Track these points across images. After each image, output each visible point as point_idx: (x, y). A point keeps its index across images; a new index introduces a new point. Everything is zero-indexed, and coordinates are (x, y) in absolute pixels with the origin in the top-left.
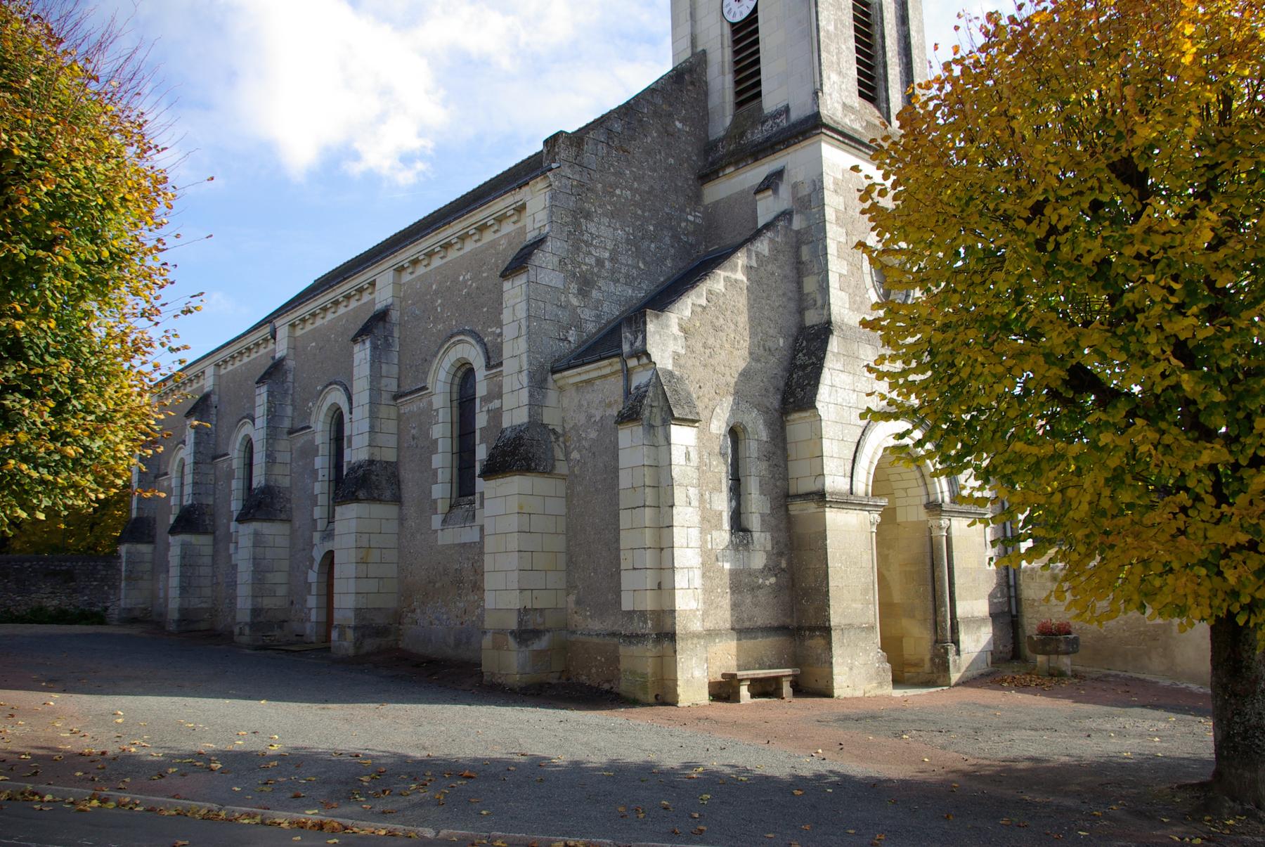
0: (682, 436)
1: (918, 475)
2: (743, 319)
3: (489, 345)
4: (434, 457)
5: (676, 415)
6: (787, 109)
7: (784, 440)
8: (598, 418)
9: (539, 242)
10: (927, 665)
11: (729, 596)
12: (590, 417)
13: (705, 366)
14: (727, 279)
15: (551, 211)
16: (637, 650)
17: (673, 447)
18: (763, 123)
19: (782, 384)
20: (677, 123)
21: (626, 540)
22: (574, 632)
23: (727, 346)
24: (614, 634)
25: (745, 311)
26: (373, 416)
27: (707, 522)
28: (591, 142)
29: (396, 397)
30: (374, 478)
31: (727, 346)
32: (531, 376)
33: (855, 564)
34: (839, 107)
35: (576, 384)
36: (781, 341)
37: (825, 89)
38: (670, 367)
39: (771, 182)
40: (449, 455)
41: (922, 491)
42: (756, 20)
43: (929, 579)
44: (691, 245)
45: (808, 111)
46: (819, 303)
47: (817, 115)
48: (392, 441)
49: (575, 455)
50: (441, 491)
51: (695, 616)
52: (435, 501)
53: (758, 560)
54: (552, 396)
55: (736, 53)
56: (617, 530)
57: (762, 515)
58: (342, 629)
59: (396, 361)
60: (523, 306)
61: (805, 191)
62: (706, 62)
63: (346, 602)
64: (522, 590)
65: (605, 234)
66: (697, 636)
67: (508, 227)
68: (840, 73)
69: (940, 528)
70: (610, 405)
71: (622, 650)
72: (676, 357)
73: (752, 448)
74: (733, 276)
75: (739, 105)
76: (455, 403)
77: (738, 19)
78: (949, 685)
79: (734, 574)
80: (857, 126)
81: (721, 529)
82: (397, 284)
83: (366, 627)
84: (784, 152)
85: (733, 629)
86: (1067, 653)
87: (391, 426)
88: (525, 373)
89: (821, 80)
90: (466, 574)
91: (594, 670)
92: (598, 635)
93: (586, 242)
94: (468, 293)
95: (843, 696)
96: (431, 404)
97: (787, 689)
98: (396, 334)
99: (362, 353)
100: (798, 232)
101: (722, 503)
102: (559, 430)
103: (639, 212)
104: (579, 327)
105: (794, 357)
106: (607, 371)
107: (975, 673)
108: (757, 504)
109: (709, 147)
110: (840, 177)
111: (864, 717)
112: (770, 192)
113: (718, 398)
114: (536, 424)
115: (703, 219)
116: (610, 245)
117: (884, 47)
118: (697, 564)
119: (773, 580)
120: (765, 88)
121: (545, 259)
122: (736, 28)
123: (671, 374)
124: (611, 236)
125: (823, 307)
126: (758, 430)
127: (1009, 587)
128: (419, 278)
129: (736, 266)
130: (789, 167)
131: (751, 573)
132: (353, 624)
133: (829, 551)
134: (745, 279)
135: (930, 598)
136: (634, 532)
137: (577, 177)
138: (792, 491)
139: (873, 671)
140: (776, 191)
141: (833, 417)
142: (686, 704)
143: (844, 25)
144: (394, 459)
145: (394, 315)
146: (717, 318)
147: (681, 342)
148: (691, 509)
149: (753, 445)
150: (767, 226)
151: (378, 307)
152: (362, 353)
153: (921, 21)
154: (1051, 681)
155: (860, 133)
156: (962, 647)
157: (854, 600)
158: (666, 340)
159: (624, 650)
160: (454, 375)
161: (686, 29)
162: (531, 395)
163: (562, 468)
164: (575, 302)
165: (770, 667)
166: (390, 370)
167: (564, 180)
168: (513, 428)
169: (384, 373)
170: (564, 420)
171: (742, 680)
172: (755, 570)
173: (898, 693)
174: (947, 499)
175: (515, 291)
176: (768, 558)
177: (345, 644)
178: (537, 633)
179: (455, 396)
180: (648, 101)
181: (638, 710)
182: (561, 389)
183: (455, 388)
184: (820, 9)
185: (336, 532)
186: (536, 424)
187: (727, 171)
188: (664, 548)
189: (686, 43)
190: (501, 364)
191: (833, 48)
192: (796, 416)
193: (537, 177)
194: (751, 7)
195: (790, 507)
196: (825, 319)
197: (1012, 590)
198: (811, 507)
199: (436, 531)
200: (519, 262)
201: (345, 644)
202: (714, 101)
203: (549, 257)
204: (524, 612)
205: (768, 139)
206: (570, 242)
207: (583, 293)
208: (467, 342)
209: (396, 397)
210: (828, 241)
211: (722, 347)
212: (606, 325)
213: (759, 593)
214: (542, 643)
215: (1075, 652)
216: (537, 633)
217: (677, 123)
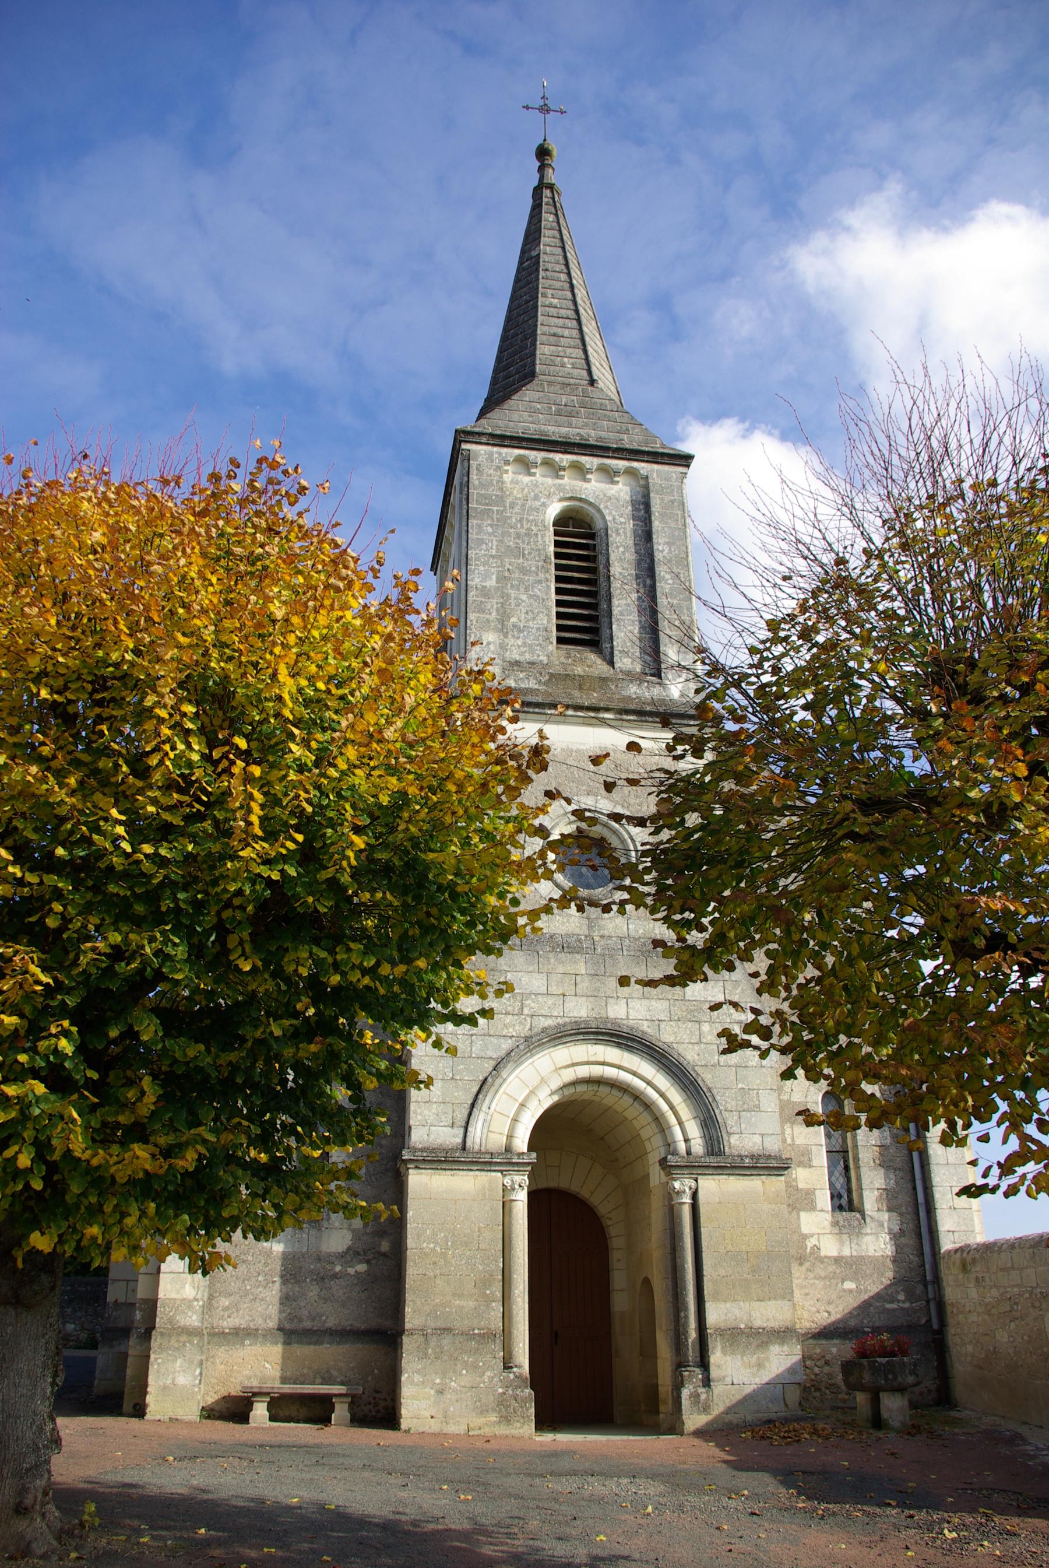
11: (278, 1285)
33: (466, 1244)
51: (190, 1307)
85: (279, 1329)
111: (439, 1460)
119: (362, 1268)
156: (714, 1373)
172: (329, 1255)
173: (548, 1437)
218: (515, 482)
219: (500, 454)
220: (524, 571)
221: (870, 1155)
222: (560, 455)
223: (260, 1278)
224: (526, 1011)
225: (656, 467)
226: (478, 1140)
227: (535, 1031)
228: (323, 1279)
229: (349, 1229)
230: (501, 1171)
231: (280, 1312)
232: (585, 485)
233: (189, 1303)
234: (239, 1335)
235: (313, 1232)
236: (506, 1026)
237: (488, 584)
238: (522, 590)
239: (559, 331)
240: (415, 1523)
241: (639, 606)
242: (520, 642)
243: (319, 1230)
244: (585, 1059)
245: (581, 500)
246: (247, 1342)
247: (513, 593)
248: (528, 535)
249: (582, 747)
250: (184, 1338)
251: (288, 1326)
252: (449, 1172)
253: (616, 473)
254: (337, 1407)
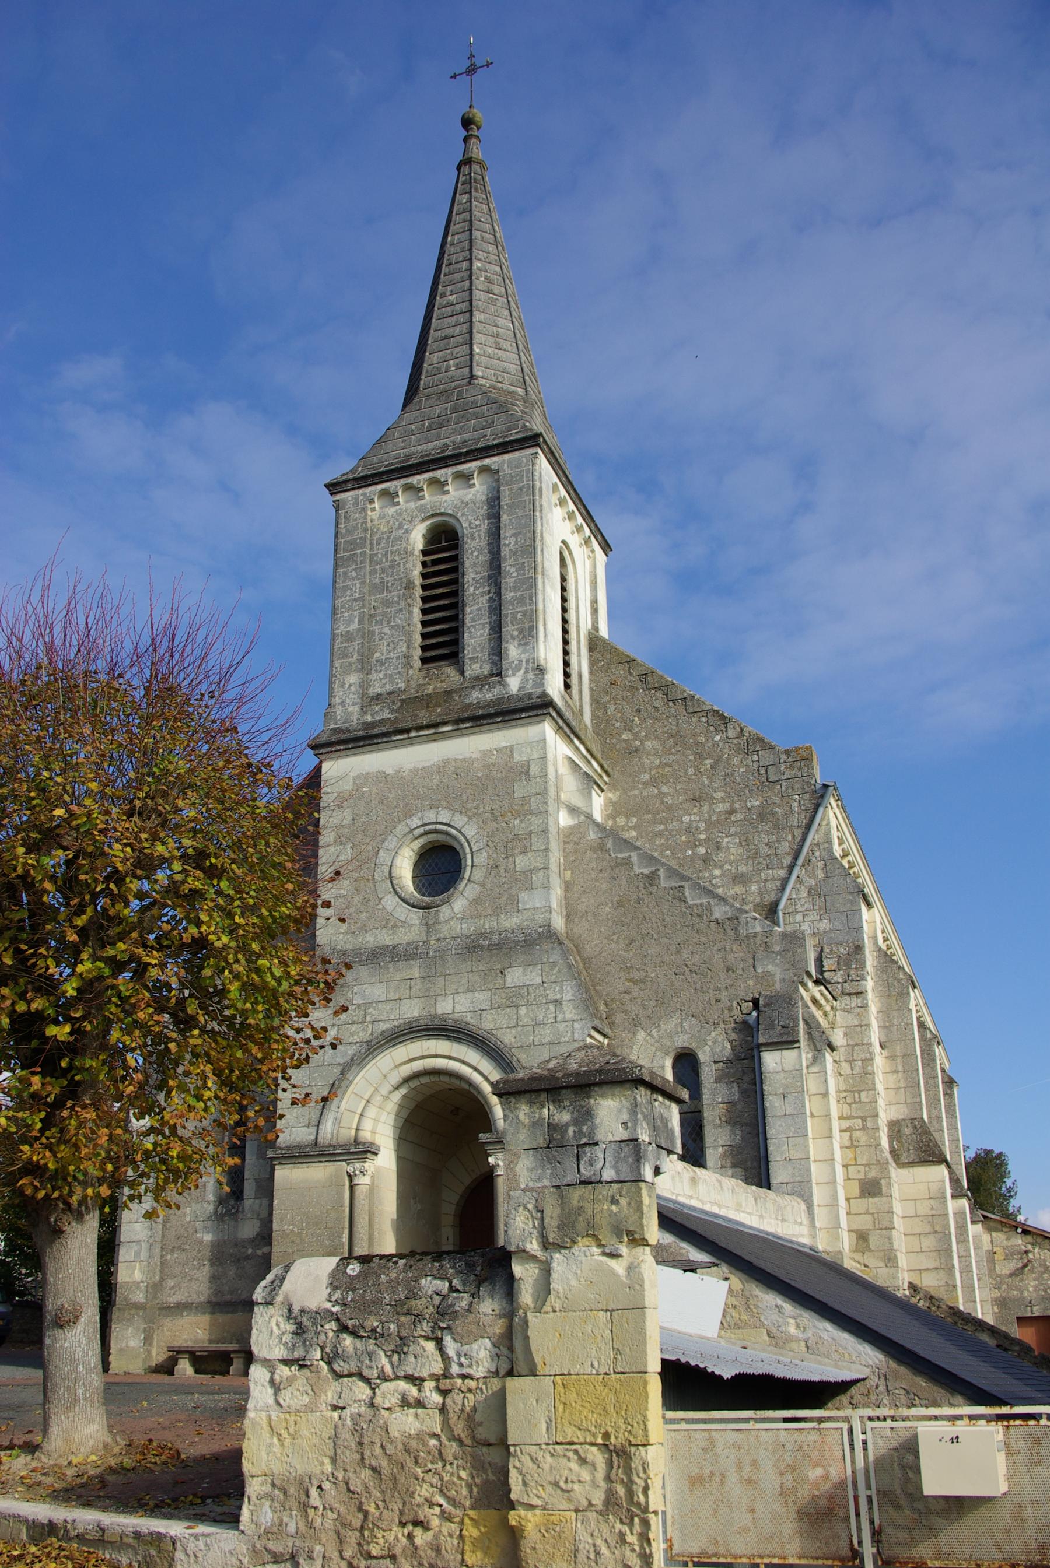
51: (138, 1287)
172: (244, 1241)
218: (382, 517)
219: (364, 494)
220: (387, 603)
221: (717, 1113)
222: (418, 477)
223: (195, 1263)
224: (368, 1019)
225: (506, 457)
226: (329, 1136)
227: (375, 1035)
228: (239, 1260)
229: (258, 1218)
231: (210, 1288)
232: (445, 498)
233: (137, 1284)
234: (181, 1307)
235: (232, 1223)
236: (352, 1035)
237: (350, 628)
238: (385, 623)
239: (449, 332)
241: (490, 607)
242: (381, 675)
243: (236, 1221)
244: (447, 1054)
245: (441, 514)
246: (185, 1313)
247: (376, 629)
248: (392, 567)
249: (428, 764)
250: (133, 1311)
251: (214, 1299)
252: (305, 1165)
254: (235, 1360)
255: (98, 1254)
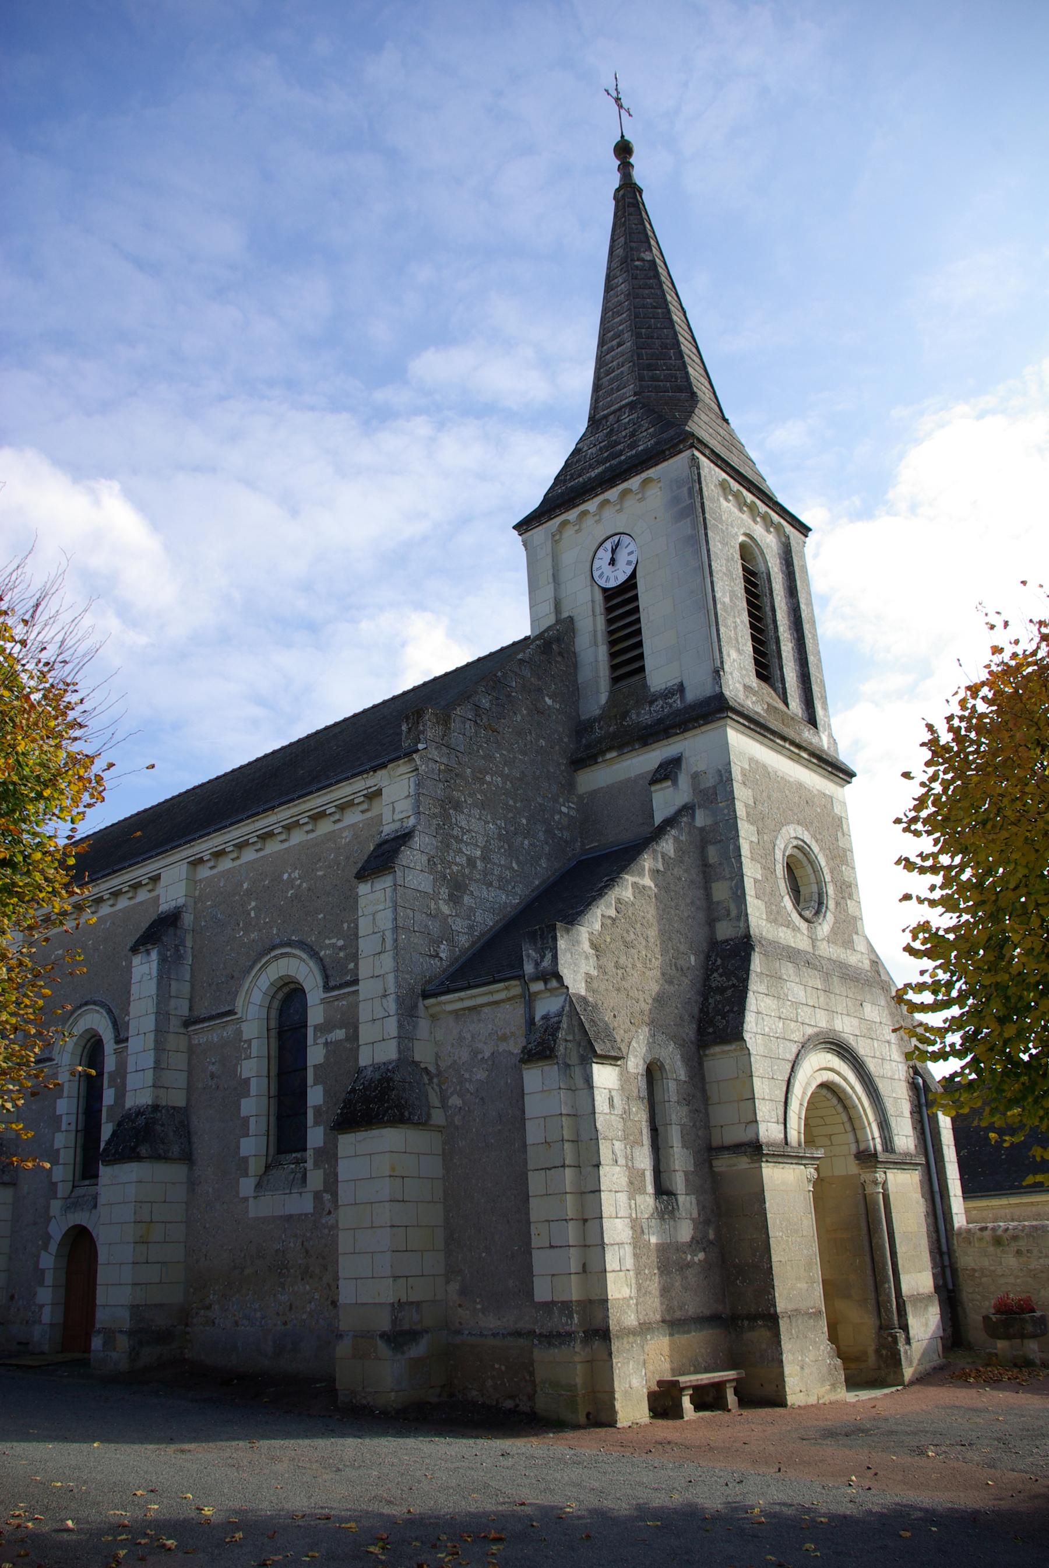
0: (605, 1077)
1: (845, 1118)
2: (653, 933)
3: (327, 960)
4: (244, 1101)
5: (599, 1052)
6: (681, 688)
7: (703, 1078)
8: (487, 1055)
9: (404, 838)
10: (872, 1359)
11: (656, 1279)
12: (475, 1053)
13: (618, 990)
14: (635, 885)
15: (418, 801)
16: (558, 1353)
17: (596, 1092)
18: (651, 703)
19: (696, 1010)
20: (547, 699)
21: (537, 1209)
22: (458, 1332)
23: (639, 965)
24: (518, 1334)
25: (655, 923)
26: (159, 1047)
27: (634, 1187)
28: (458, 719)
29: (187, 1023)
30: (158, 1128)
31: (639, 965)
32: (400, 1001)
34: (741, 688)
35: (456, 1013)
36: (693, 958)
37: (726, 667)
38: (583, 993)
39: (668, 771)
40: (265, 1100)
41: (850, 1137)
42: (635, 586)
43: (867, 1249)
44: (566, 841)
45: (708, 691)
46: (734, 913)
47: (720, 697)
48: (181, 1080)
49: (455, 1101)
50: (253, 1146)
51: (629, 1306)
52: (245, 1160)
53: (685, 1232)
54: (424, 1025)
55: (610, 622)
56: (525, 1198)
57: (686, 1173)
58: (110, 1335)
59: (188, 977)
60: (389, 914)
61: (709, 782)
62: (573, 630)
63: (116, 1293)
64: (396, 1278)
65: (476, 827)
66: (631, 1332)
67: (353, 817)
68: (738, 650)
69: (875, 1183)
70: (504, 1038)
71: (538, 1354)
72: (589, 979)
73: (671, 1089)
74: (641, 882)
75: (615, 680)
76: (273, 1033)
77: (612, 584)
78: (902, 1383)
79: (662, 1249)
80: (758, 709)
81: (644, 1193)
82: (191, 881)
83: (146, 1331)
84: (681, 737)
85: (663, 1321)
86: (1033, 1336)
87: (179, 1061)
88: (391, 999)
89: (721, 657)
90: (314, 1253)
91: (489, 1383)
92: (494, 1335)
93: (456, 838)
94: (296, 896)
95: (797, 1403)
96: (239, 1032)
97: (731, 1399)
98: (189, 944)
99: (144, 969)
100: (702, 829)
101: (644, 1161)
102: (432, 1069)
103: (511, 802)
104: (451, 941)
105: (707, 978)
106: (502, 995)
107: (928, 1366)
108: (680, 1160)
109: (582, 728)
110: (747, 767)
112: (669, 783)
113: (633, 1029)
114: (406, 1061)
115: (578, 810)
116: (481, 842)
117: (775, 621)
118: (627, 1238)
119: (701, 1256)
120: (649, 662)
121: (413, 858)
122: (609, 594)
123: (584, 999)
124: (482, 831)
125: (738, 918)
126: (677, 1069)
127: (941, 1254)
128: (223, 874)
129: (643, 869)
130: (686, 754)
131: (679, 1248)
132: (127, 1326)
133: (768, 1216)
134: (653, 886)
135: (869, 1272)
136: (547, 1203)
137: (445, 760)
138: (716, 1142)
139: (824, 1370)
140: (675, 782)
141: (761, 1050)
142: (626, 1424)
143: (737, 597)
144: (182, 1103)
145: (188, 919)
146: (628, 932)
147: (593, 961)
148: (618, 1169)
149: (672, 1086)
150: (670, 822)
151: (164, 907)
152: (144, 969)
153: (809, 593)
154: (1021, 1372)
155: (764, 717)
156: (912, 1332)
157: (798, 1279)
158: (579, 959)
159: (541, 1355)
160: (273, 997)
161: (549, 592)
162: (400, 1026)
163: (438, 1117)
164: (445, 909)
165: (707, 1370)
166: (181, 988)
167: (431, 764)
168: (376, 1067)
169: (172, 994)
170: (437, 1056)
171: (684, 1389)
172: (683, 1244)
173: (851, 1397)
174: (879, 1148)
175: (374, 899)
176: (695, 1228)
177: (115, 1355)
178: (412, 1336)
179: (273, 1024)
180: (516, 674)
181: (570, 1435)
182: (434, 1017)
183: (274, 1014)
184: (715, 579)
185: (102, 1200)
186: (406, 1061)
187: (608, 756)
188: (590, 1219)
189: (548, 608)
190: (356, 982)
191: (730, 622)
192: (717, 1049)
193: (398, 758)
194: (629, 573)
195: (715, 1163)
196: (741, 932)
197: (946, 1258)
198: (743, 1163)
199: (246, 1199)
200: (382, 858)
201: (115, 1355)
202: (585, 674)
203: (418, 855)
204: (398, 1306)
205: (660, 721)
206: (440, 838)
207: (454, 900)
208: (295, 956)
209: (187, 1023)
210: (741, 840)
211: (634, 966)
212: (479, 938)
213: (689, 1272)
214: (418, 1350)
215: (1043, 1334)
216: (412, 1336)
217: (547, 699)
230: (804, 1165)
231: (662, 1304)
235: (672, 1223)
240: (271, 1517)
246: (649, 1337)
250: (631, 1339)
251: (668, 1318)
253: (745, 504)
255: (337, 1244)
